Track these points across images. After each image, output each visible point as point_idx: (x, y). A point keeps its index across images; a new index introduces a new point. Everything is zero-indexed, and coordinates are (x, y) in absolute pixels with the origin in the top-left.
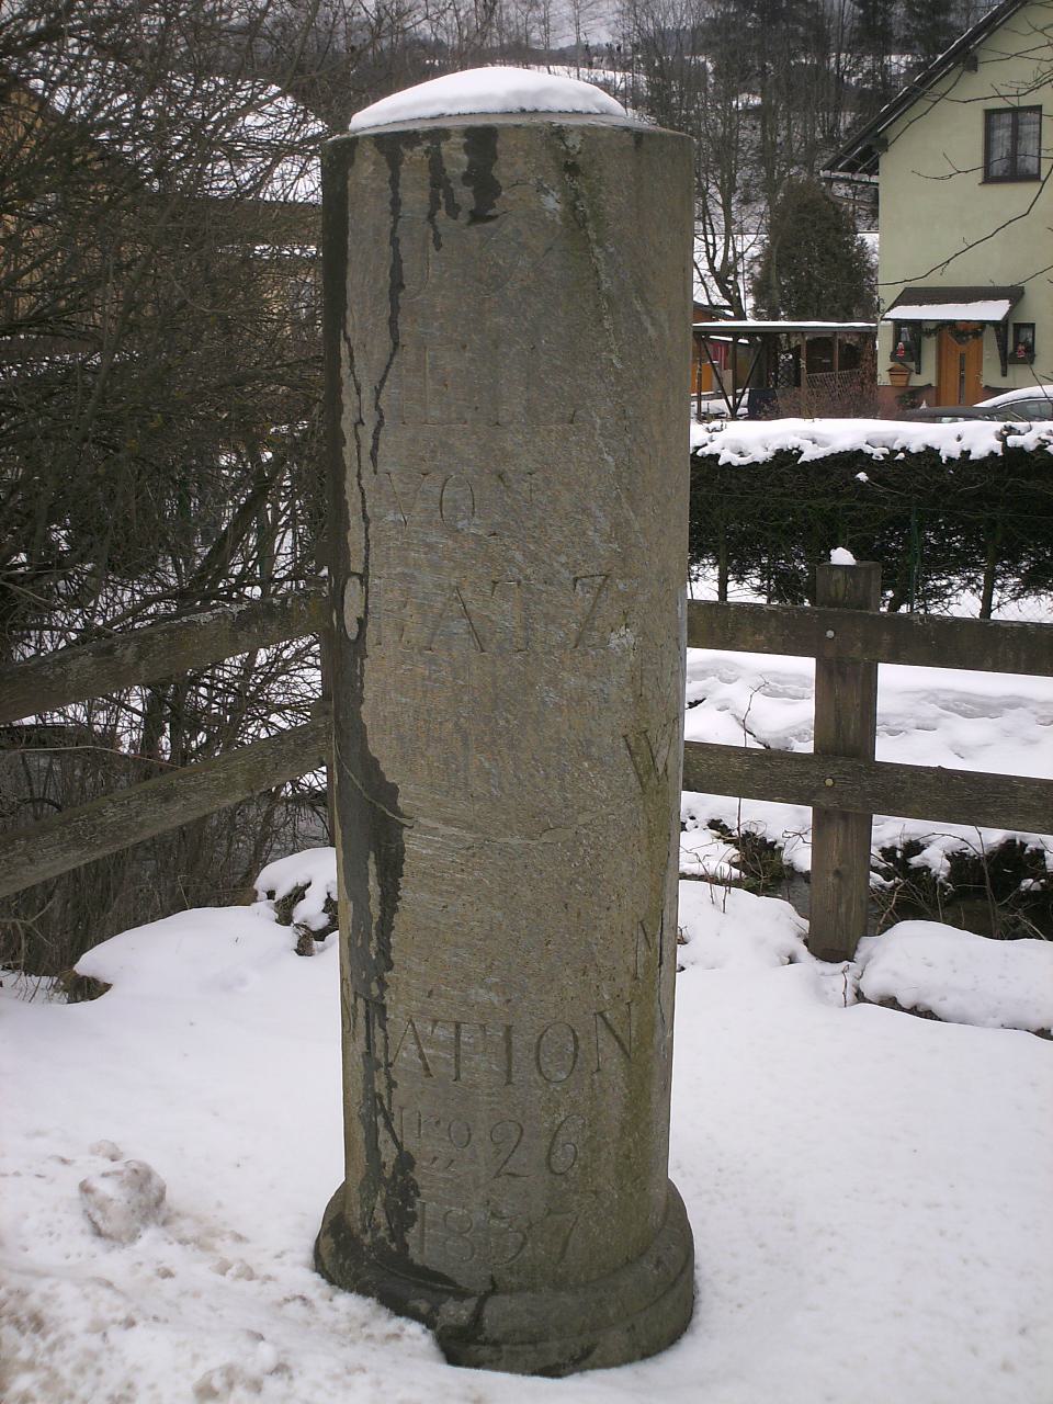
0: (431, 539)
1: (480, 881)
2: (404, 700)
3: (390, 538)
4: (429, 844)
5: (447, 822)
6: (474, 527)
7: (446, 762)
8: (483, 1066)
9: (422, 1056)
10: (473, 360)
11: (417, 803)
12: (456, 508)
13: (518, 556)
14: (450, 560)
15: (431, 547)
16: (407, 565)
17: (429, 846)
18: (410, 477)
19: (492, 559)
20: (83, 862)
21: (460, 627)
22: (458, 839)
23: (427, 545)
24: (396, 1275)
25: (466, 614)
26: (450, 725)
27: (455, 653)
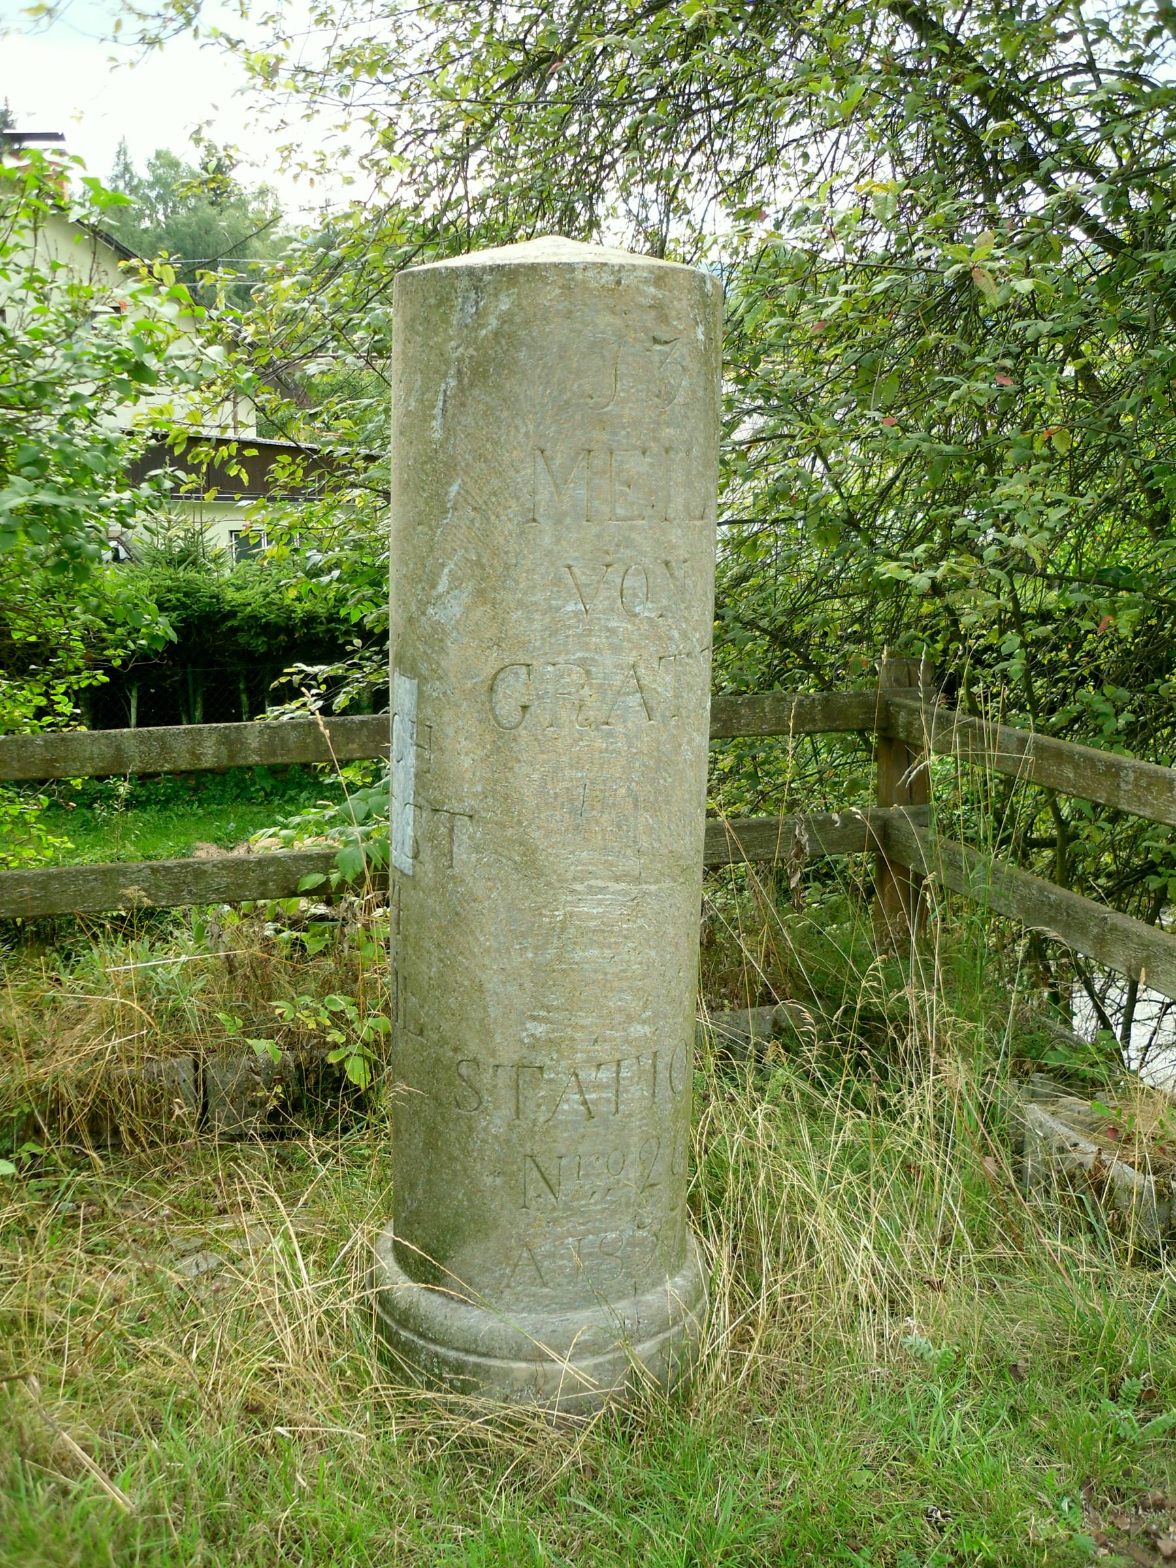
0: (613, 624)
1: (641, 927)
2: (579, 775)
3: (570, 627)
4: (600, 903)
5: (617, 879)
6: (646, 611)
7: (619, 827)
8: (638, 1094)
9: (585, 1103)
10: (651, 465)
11: (590, 868)
12: (635, 595)
13: (676, 634)
14: (629, 641)
15: (612, 631)
16: (588, 650)
17: (599, 905)
18: (594, 569)
19: (660, 638)
20: (1118, 919)
21: (634, 701)
22: (627, 894)
23: (608, 630)
24: (1052, 70)
25: (641, 688)
26: (623, 791)
27: (629, 725)
